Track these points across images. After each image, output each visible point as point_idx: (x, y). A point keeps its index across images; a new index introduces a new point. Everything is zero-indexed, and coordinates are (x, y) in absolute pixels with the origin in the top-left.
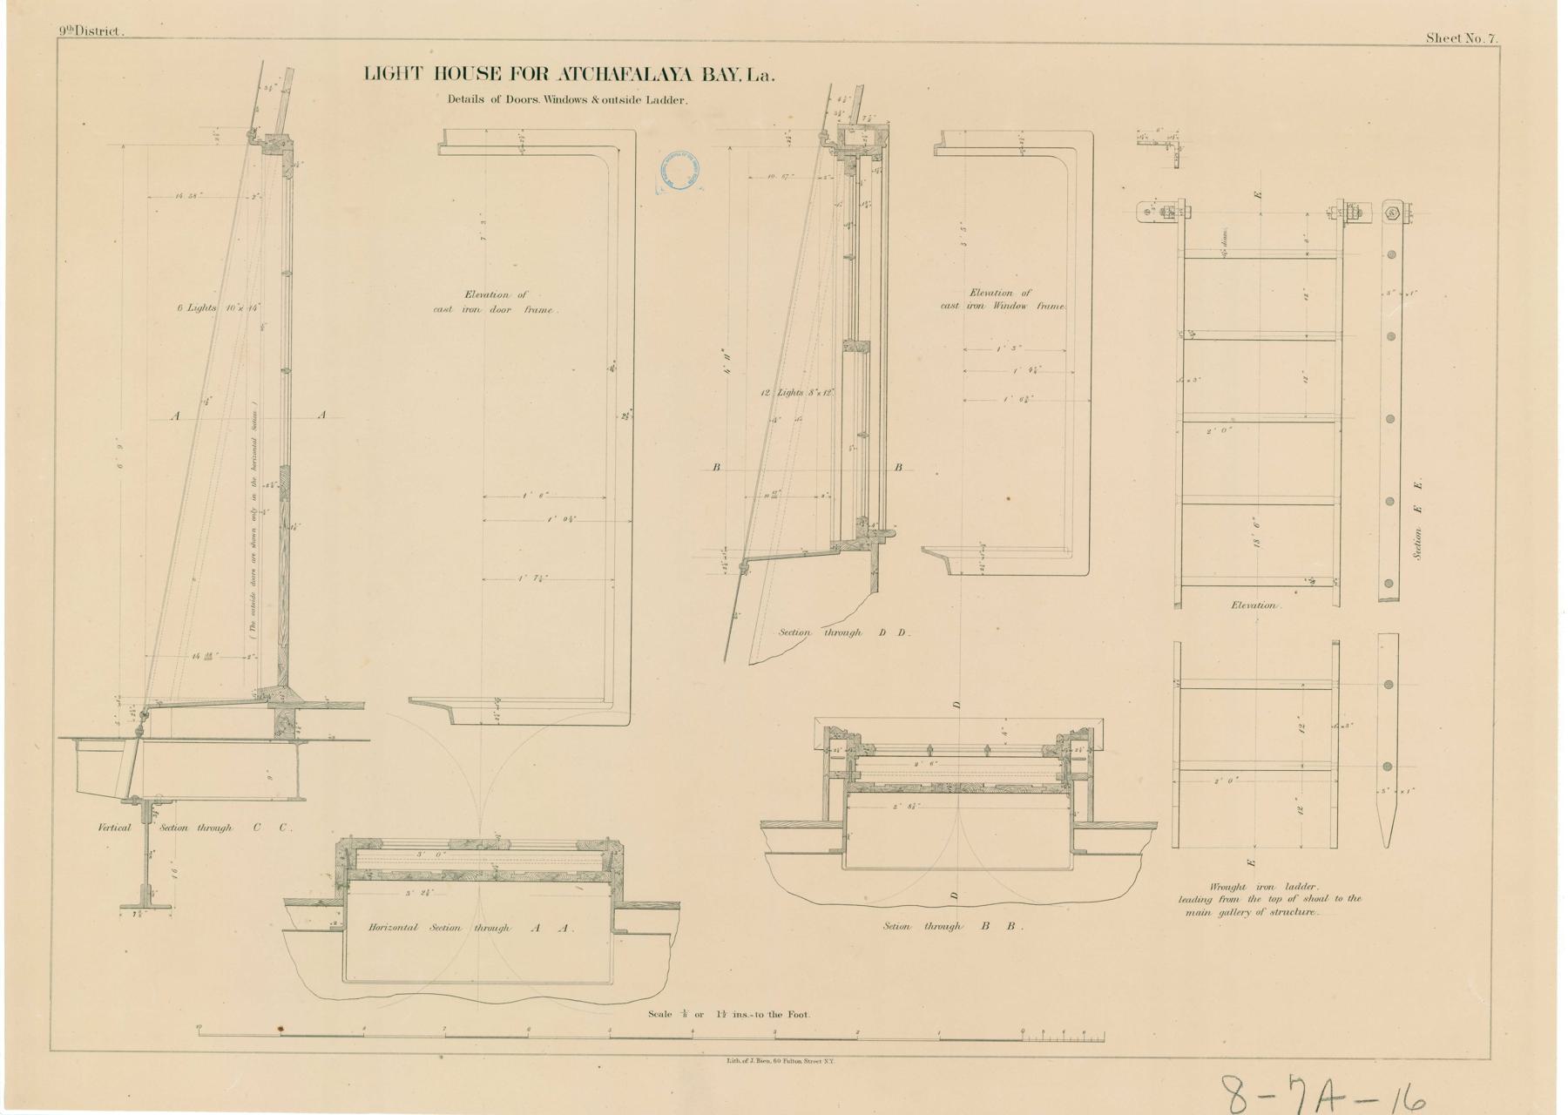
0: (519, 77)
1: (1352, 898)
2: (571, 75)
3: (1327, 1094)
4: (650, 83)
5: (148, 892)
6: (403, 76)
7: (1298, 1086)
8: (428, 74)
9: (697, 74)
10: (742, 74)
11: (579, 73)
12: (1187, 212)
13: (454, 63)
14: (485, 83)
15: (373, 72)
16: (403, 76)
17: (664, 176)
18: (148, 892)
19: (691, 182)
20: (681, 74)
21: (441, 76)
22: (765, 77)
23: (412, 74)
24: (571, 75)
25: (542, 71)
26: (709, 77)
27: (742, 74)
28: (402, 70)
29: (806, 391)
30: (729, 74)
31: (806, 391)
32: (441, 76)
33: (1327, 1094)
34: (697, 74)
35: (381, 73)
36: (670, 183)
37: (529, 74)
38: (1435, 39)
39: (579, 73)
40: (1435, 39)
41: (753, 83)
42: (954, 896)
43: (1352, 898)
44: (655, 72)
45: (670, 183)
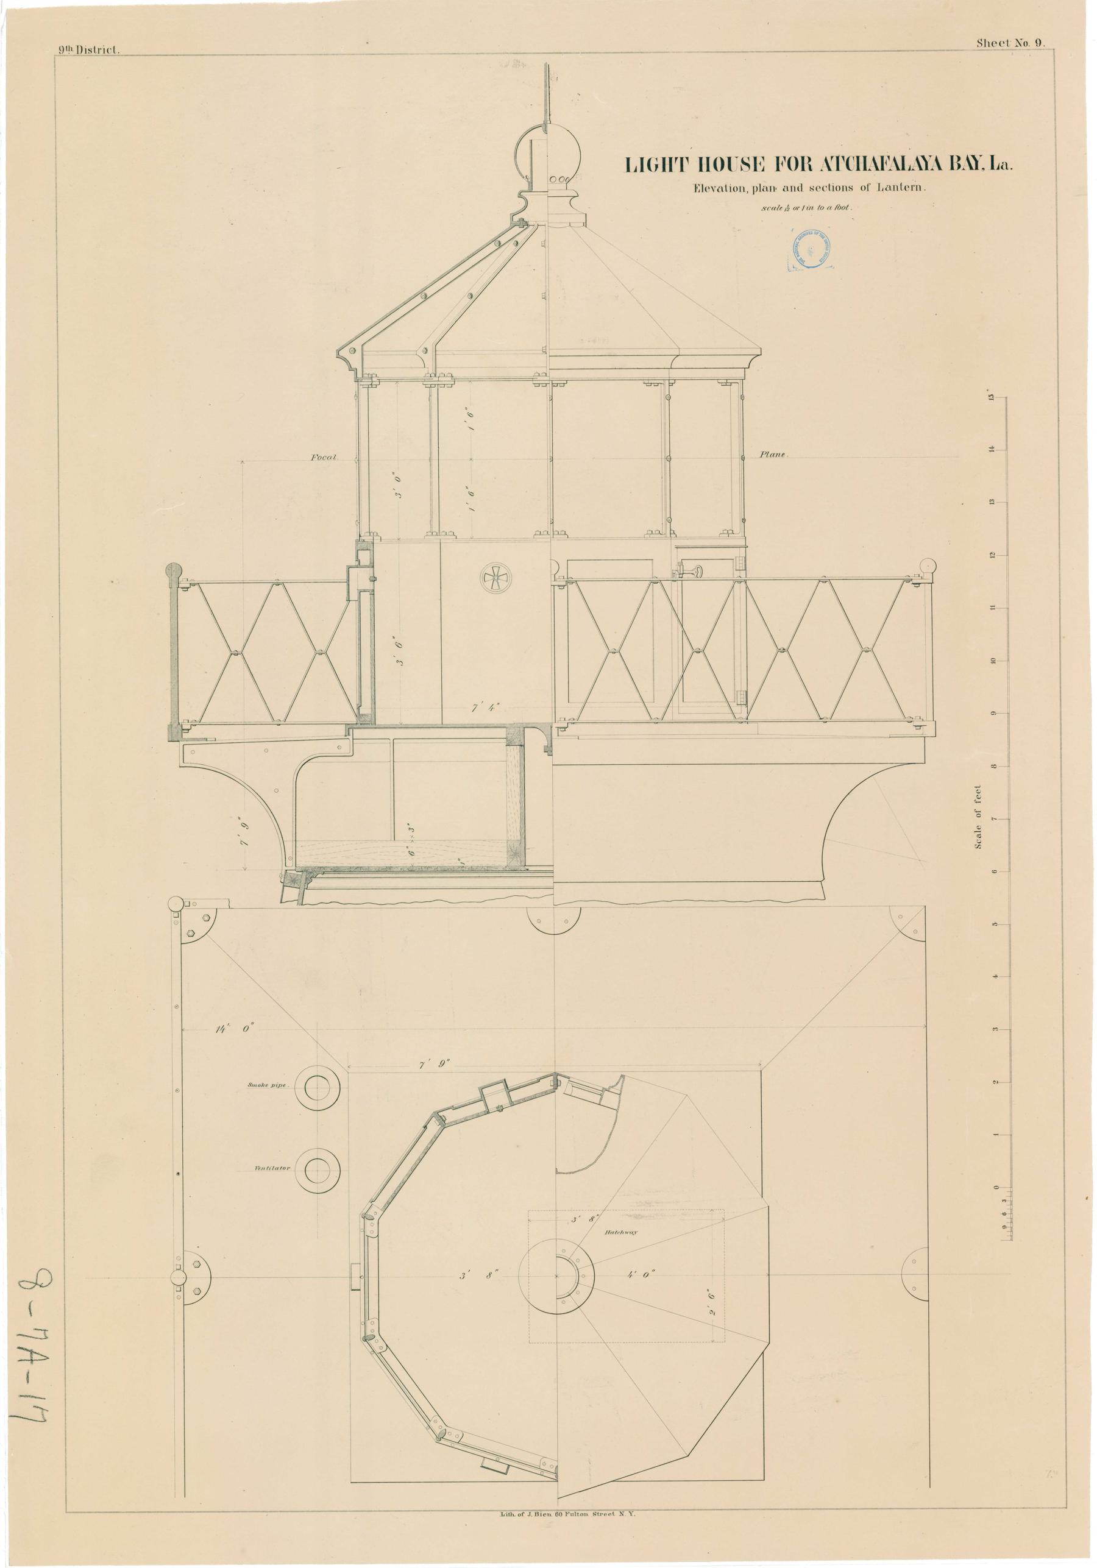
0: (784, 168)
3: (35, 1357)
4: (906, 172)
5: (518, 850)
9: (945, 163)
10: (984, 162)
11: (842, 164)
12: (289, 880)
14: (749, 173)
15: (635, 163)
17: (796, 253)
18: (518, 850)
19: (822, 261)
20: (932, 163)
22: (1004, 166)
23: (676, 166)
27: (984, 162)
29: (975, 822)
30: (973, 163)
31: (975, 822)
33: (35, 1357)
34: (945, 163)
35: (645, 165)
36: (801, 261)
37: (853, 164)
39: (842, 164)
41: (995, 171)
44: (910, 161)
45: (801, 261)
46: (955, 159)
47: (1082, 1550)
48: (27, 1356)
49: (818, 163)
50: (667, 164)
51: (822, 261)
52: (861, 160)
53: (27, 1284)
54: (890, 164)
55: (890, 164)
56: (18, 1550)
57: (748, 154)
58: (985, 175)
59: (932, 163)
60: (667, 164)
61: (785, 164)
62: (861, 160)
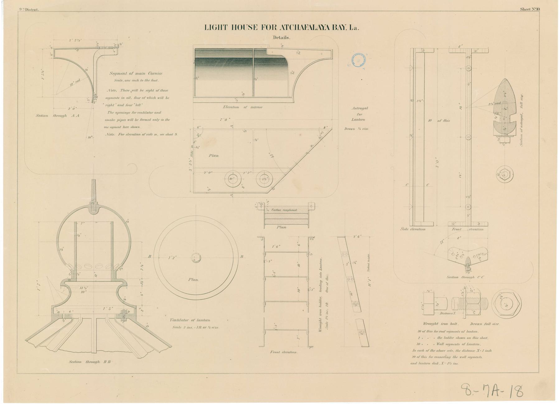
1: (445, 121)
2: (285, 27)
3: (495, 389)
4: (315, 30)
6: (220, 28)
7: (486, 388)
8: (229, 28)
11: (288, 27)
13: (239, 23)
15: (208, 27)
16: (220, 28)
19: (361, 66)
20: (325, 27)
21: (234, 28)
22: (356, 29)
23: (223, 27)
24: (285, 27)
25: (274, 26)
26: (335, 28)
27: (347, 27)
28: (220, 26)
29: (207, 174)
30: (342, 27)
31: (207, 174)
32: (234, 28)
33: (495, 389)
35: (211, 27)
38: (523, 10)
39: (288, 27)
40: (523, 10)
42: (242, 256)
43: (445, 121)
44: (316, 27)
46: (335, 26)
47: (553, 399)
48: (495, 392)
49: (279, 27)
50: (220, 27)
51: (361, 66)
52: (297, 26)
53: (468, 392)
54: (308, 28)
55: (308, 28)
56: (7, 398)
57: (251, 24)
58: (347, 32)
59: (325, 27)
60: (220, 27)
61: (265, 27)
62: (297, 26)
